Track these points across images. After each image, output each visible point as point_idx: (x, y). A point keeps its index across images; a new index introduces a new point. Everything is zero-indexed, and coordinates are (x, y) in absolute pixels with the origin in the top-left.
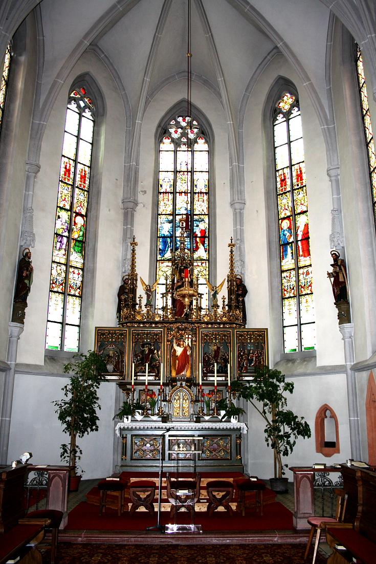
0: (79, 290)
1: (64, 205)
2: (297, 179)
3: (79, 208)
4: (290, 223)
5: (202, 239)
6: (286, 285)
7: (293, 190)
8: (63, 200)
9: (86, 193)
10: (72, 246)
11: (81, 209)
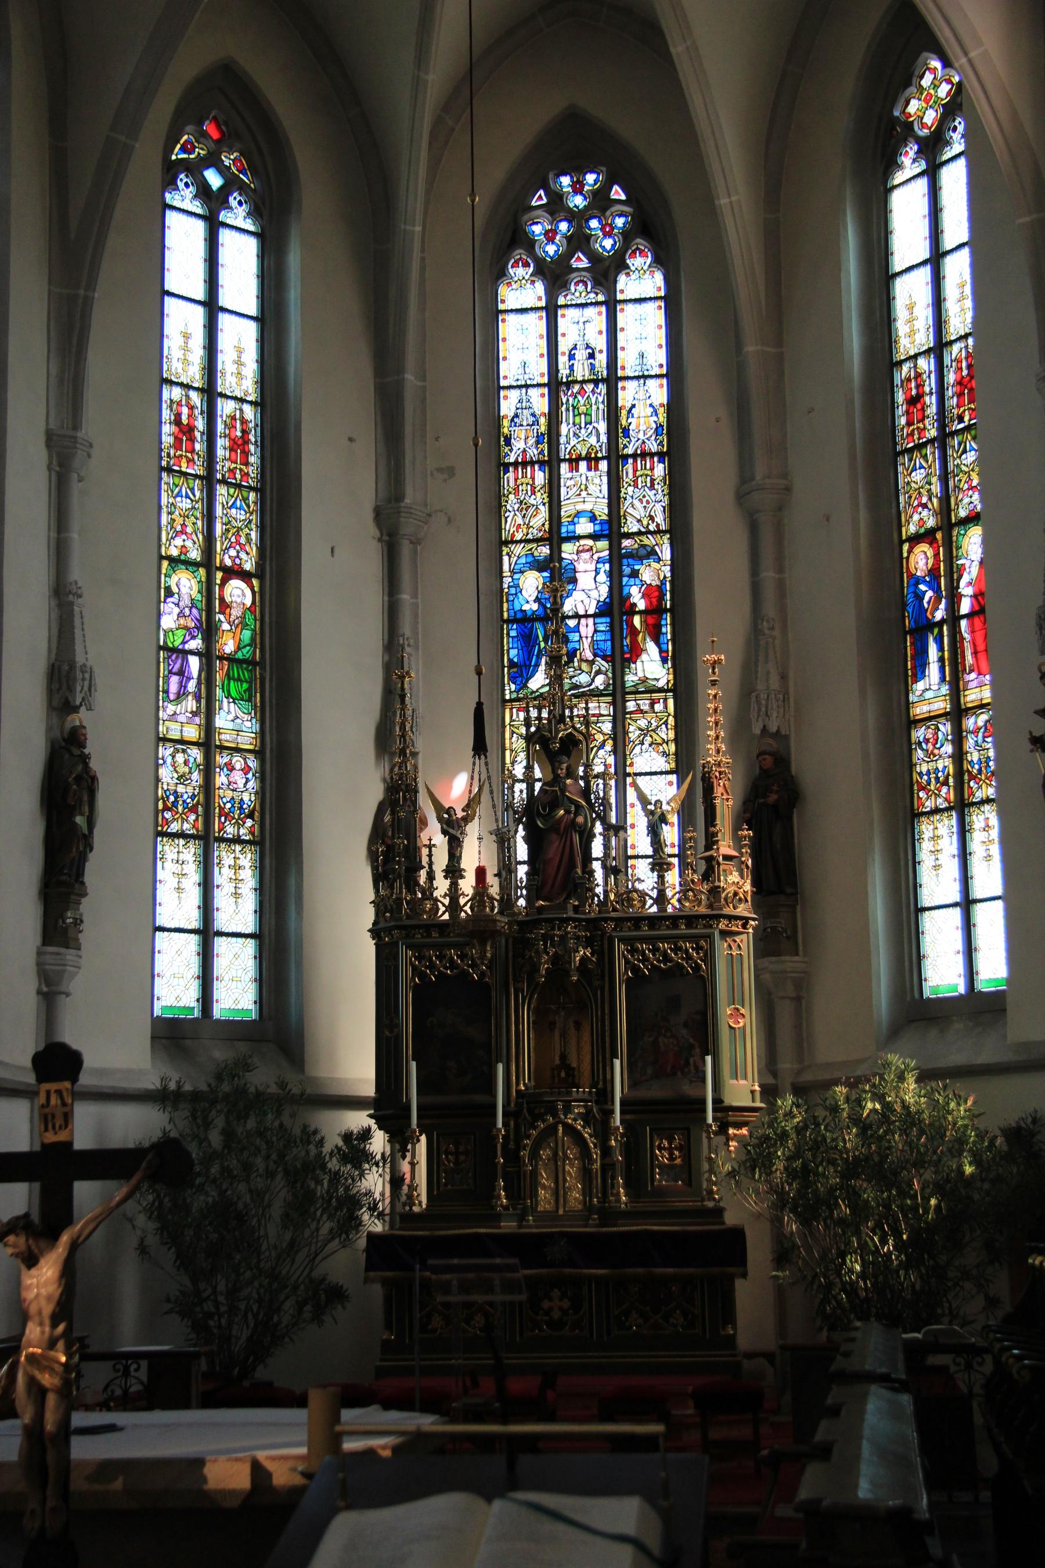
0: (249, 823)
1: (184, 549)
2: (960, 395)
3: (233, 553)
4: (936, 555)
5: (651, 620)
6: (924, 768)
8: (177, 534)
9: (252, 496)
11: (243, 555)
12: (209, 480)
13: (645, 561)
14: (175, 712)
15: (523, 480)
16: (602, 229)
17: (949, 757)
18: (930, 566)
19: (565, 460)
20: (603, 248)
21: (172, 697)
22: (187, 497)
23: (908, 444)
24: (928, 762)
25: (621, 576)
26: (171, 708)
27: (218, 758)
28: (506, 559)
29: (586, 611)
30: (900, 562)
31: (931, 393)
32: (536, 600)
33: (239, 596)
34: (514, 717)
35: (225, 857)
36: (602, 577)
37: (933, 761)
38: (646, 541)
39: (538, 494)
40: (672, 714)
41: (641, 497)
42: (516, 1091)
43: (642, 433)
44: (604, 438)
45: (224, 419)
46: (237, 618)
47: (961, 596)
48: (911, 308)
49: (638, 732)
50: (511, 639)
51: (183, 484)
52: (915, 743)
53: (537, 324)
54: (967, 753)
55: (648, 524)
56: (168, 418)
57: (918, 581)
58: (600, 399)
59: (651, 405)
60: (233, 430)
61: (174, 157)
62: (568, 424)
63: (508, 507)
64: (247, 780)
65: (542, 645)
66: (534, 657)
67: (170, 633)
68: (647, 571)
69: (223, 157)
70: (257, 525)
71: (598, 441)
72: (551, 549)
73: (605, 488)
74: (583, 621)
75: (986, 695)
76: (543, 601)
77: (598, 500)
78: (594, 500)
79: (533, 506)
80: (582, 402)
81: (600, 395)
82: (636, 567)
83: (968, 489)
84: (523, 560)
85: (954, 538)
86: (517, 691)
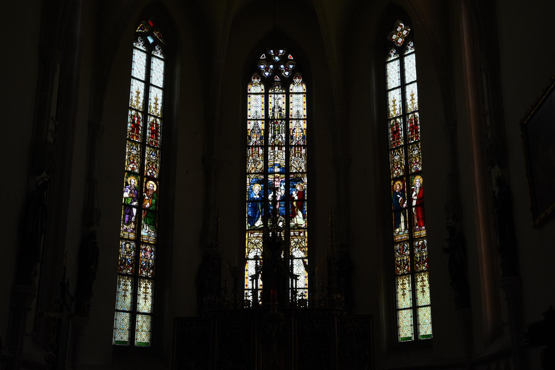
2: (412, 131)
3: (131, 166)
4: (404, 185)
7: (406, 146)
8: (132, 163)
11: (154, 172)
12: (143, 145)
13: (298, 183)
14: (127, 228)
15: (255, 152)
16: (285, 69)
17: (408, 255)
18: (401, 188)
19: (270, 146)
20: (285, 74)
21: (126, 222)
22: (135, 150)
23: (393, 147)
24: (400, 257)
25: (289, 187)
27: (141, 246)
28: (248, 179)
30: (390, 188)
31: (401, 130)
32: (259, 194)
33: (152, 187)
34: (249, 236)
35: (142, 284)
37: (402, 257)
38: (299, 176)
39: (260, 157)
40: (307, 237)
41: (297, 160)
43: (297, 138)
44: (284, 139)
45: (150, 123)
46: (151, 195)
47: (413, 199)
48: (394, 101)
49: (294, 243)
50: (249, 208)
51: (134, 145)
52: (396, 250)
53: (261, 99)
54: (396, 258)
55: (299, 170)
56: (130, 121)
57: (397, 194)
58: (283, 126)
59: (301, 129)
60: (153, 127)
61: (137, 31)
62: (272, 133)
63: (249, 161)
65: (260, 210)
66: (257, 215)
67: (127, 199)
69: (154, 33)
70: (159, 161)
71: (282, 140)
73: (284, 156)
75: (424, 233)
77: (282, 160)
78: (280, 160)
79: (258, 161)
80: (277, 126)
81: (283, 124)
82: (295, 185)
83: (415, 163)
84: (254, 180)
85: (410, 179)
86: (250, 227)
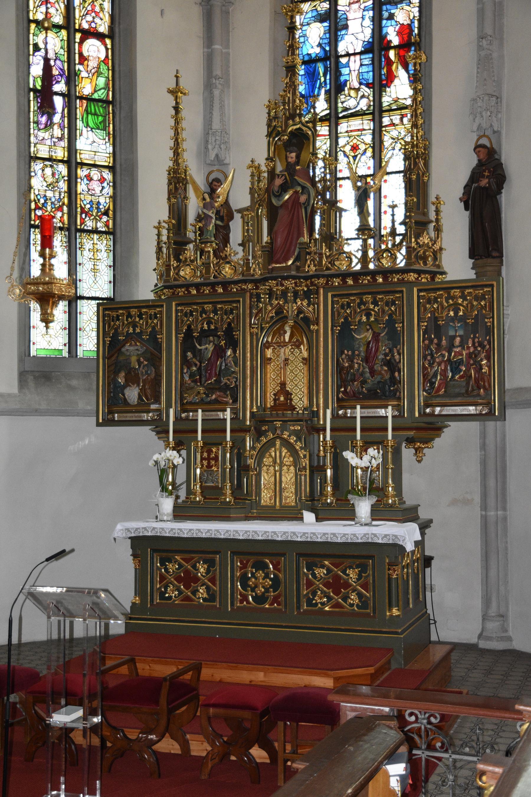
3: (89, 18)
5: (402, 52)
10: (79, 116)
11: (97, 20)
13: (399, 6)
25: (381, 19)
26: (41, 134)
29: (355, 50)
32: (320, 45)
35: (86, 243)
36: (368, 22)
42: (250, 412)
64: (103, 188)
65: (323, 79)
68: (400, 13)
72: (330, 4)
74: (352, 58)
76: (323, 45)
82: (392, 11)
84: (309, 15)
